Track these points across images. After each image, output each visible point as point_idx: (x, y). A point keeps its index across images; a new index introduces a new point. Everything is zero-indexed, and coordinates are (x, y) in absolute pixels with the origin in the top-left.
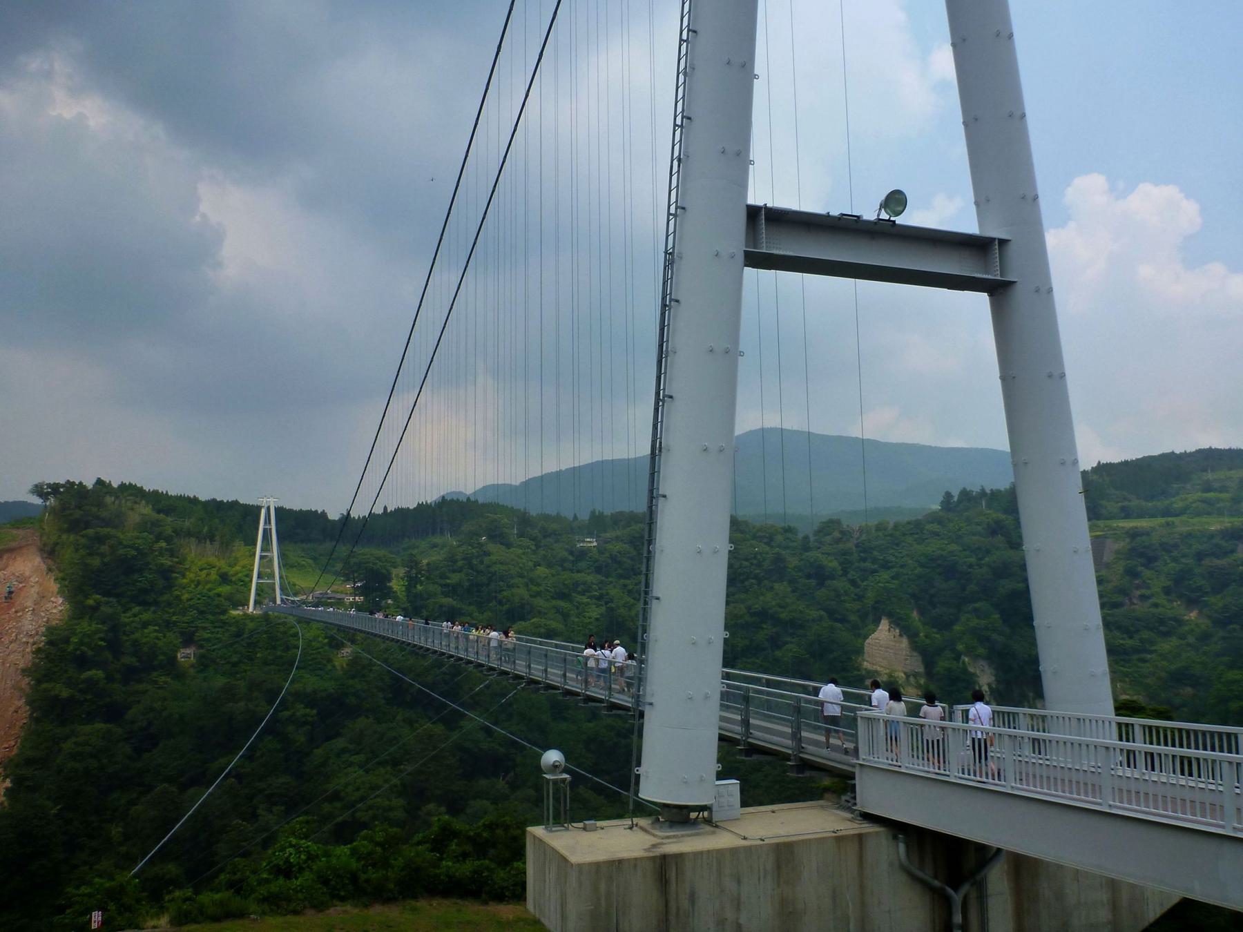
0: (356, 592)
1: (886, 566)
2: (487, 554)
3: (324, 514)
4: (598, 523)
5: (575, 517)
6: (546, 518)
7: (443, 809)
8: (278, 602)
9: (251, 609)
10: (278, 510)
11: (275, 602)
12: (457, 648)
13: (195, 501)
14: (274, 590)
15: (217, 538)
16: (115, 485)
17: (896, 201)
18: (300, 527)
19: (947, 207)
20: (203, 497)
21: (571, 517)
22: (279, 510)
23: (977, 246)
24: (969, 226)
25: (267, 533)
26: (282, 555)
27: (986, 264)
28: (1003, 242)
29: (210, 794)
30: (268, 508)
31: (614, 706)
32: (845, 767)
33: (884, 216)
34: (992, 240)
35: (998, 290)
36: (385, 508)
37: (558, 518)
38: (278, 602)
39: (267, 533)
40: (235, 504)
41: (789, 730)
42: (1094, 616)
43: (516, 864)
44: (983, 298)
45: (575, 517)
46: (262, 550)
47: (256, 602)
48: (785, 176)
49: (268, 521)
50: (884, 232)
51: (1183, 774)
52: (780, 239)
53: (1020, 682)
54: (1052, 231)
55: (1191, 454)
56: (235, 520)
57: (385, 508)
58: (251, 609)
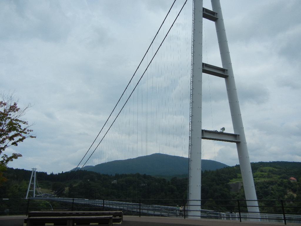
0: (55, 194)
3: (46, 173)
4: (117, 177)
5: (111, 175)
6: (104, 175)
8: (34, 196)
11: (33, 196)
17: (223, 129)
18: (41, 176)
19: (230, 129)
20: (15, 168)
23: (223, 70)
24: (221, 67)
25: (33, 178)
26: (36, 184)
27: (237, 138)
28: (239, 135)
33: (221, 131)
34: (237, 135)
35: (238, 143)
36: (62, 172)
37: (107, 175)
38: (34, 196)
39: (33, 178)
42: (253, 185)
44: (235, 144)
45: (111, 175)
47: (28, 196)
48: (206, 126)
49: (34, 175)
50: (221, 133)
51: (280, 222)
52: (207, 135)
55: (257, 163)
57: (62, 172)
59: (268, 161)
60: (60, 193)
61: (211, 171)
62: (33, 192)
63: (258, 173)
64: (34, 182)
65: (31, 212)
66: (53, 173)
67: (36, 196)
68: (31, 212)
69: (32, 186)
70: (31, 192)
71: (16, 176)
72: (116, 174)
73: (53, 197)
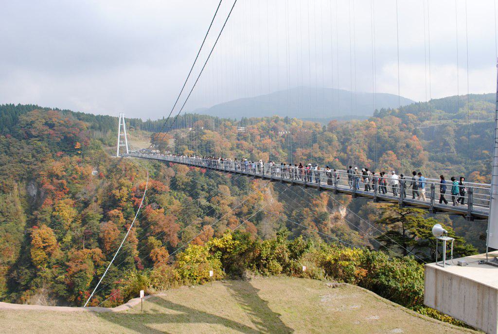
3: (140, 120)
8: (128, 153)
9: (118, 156)
12: (442, 199)
13: (92, 115)
14: (126, 148)
16: (62, 110)
18: (133, 124)
25: (122, 127)
29: (118, 254)
30: (122, 119)
31: (294, 184)
32: (460, 211)
36: (163, 117)
38: (128, 153)
39: (122, 127)
41: (473, 206)
54: (494, 93)
57: (163, 117)
58: (118, 156)
59: (481, 93)
60: (162, 146)
61: (391, 109)
62: (126, 147)
63: (125, 150)
64: (123, 123)
65: (181, 313)
66: (150, 120)
67: (130, 152)
68: (181, 313)
69: (122, 139)
70: (123, 147)
71: (98, 125)
72: (243, 118)
73: (154, 154)
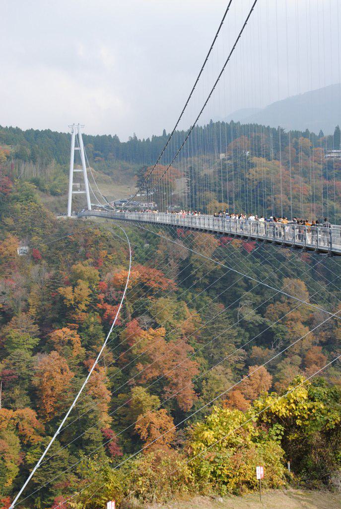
1: (62, 401)
2: (252, 165)
3: (116, 139)
5: (321, 133)
7: (37, 395)
8: (90, 208)
10: (83, 135)
11: (87, 209)
13: (18, 130)
15: (39, 160)
18: (102, 148)
20: (24, 129)
21: (317, 134)
22: (83, 135)
25: (77, 153)
30: (77, 136)
38: (90, 208)
39: (77, 153)
40: (48, 133)
43: (49, 437)
45: (321, 133)
46: (74, 168)
53: (287, 468)
56: (46, 147)
57: (164, 131)
62: (85, 195)
69: (78, 178)
